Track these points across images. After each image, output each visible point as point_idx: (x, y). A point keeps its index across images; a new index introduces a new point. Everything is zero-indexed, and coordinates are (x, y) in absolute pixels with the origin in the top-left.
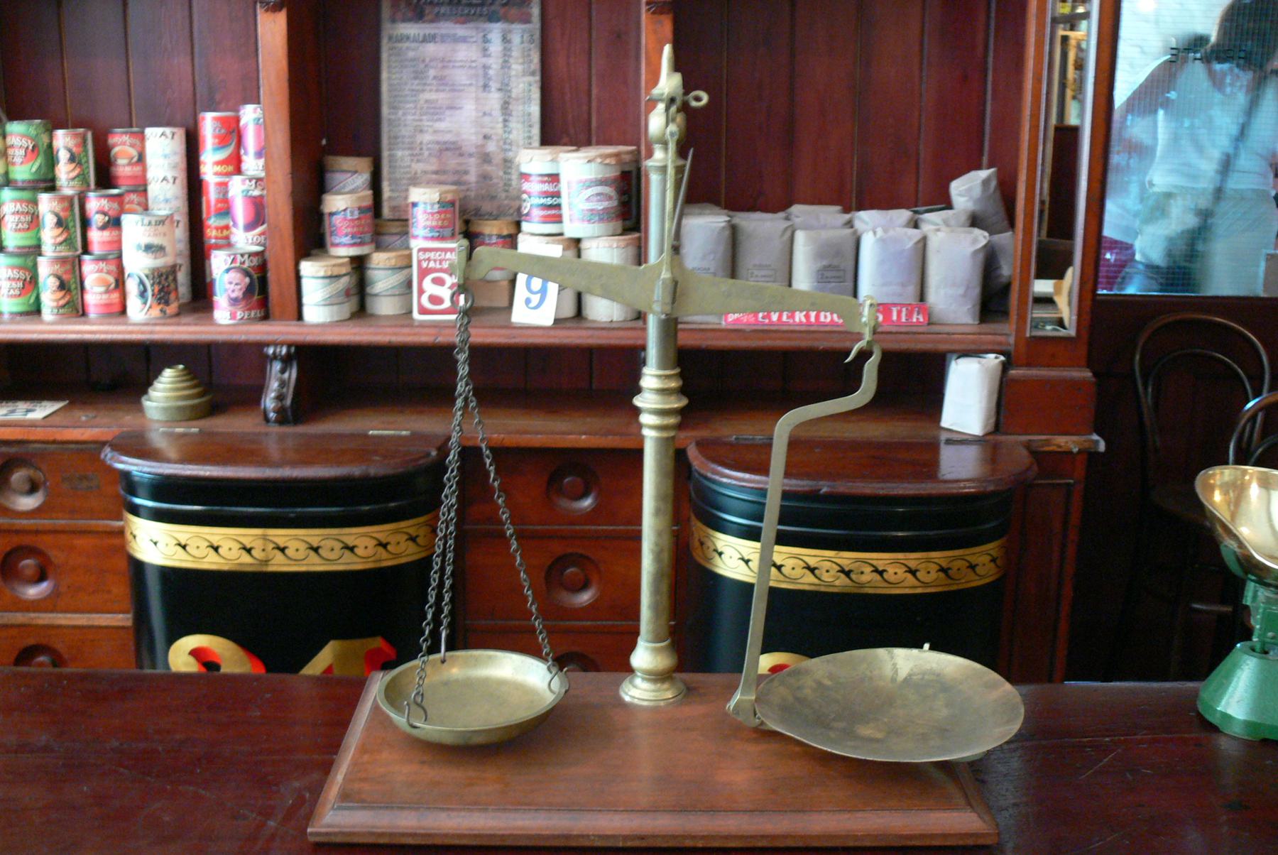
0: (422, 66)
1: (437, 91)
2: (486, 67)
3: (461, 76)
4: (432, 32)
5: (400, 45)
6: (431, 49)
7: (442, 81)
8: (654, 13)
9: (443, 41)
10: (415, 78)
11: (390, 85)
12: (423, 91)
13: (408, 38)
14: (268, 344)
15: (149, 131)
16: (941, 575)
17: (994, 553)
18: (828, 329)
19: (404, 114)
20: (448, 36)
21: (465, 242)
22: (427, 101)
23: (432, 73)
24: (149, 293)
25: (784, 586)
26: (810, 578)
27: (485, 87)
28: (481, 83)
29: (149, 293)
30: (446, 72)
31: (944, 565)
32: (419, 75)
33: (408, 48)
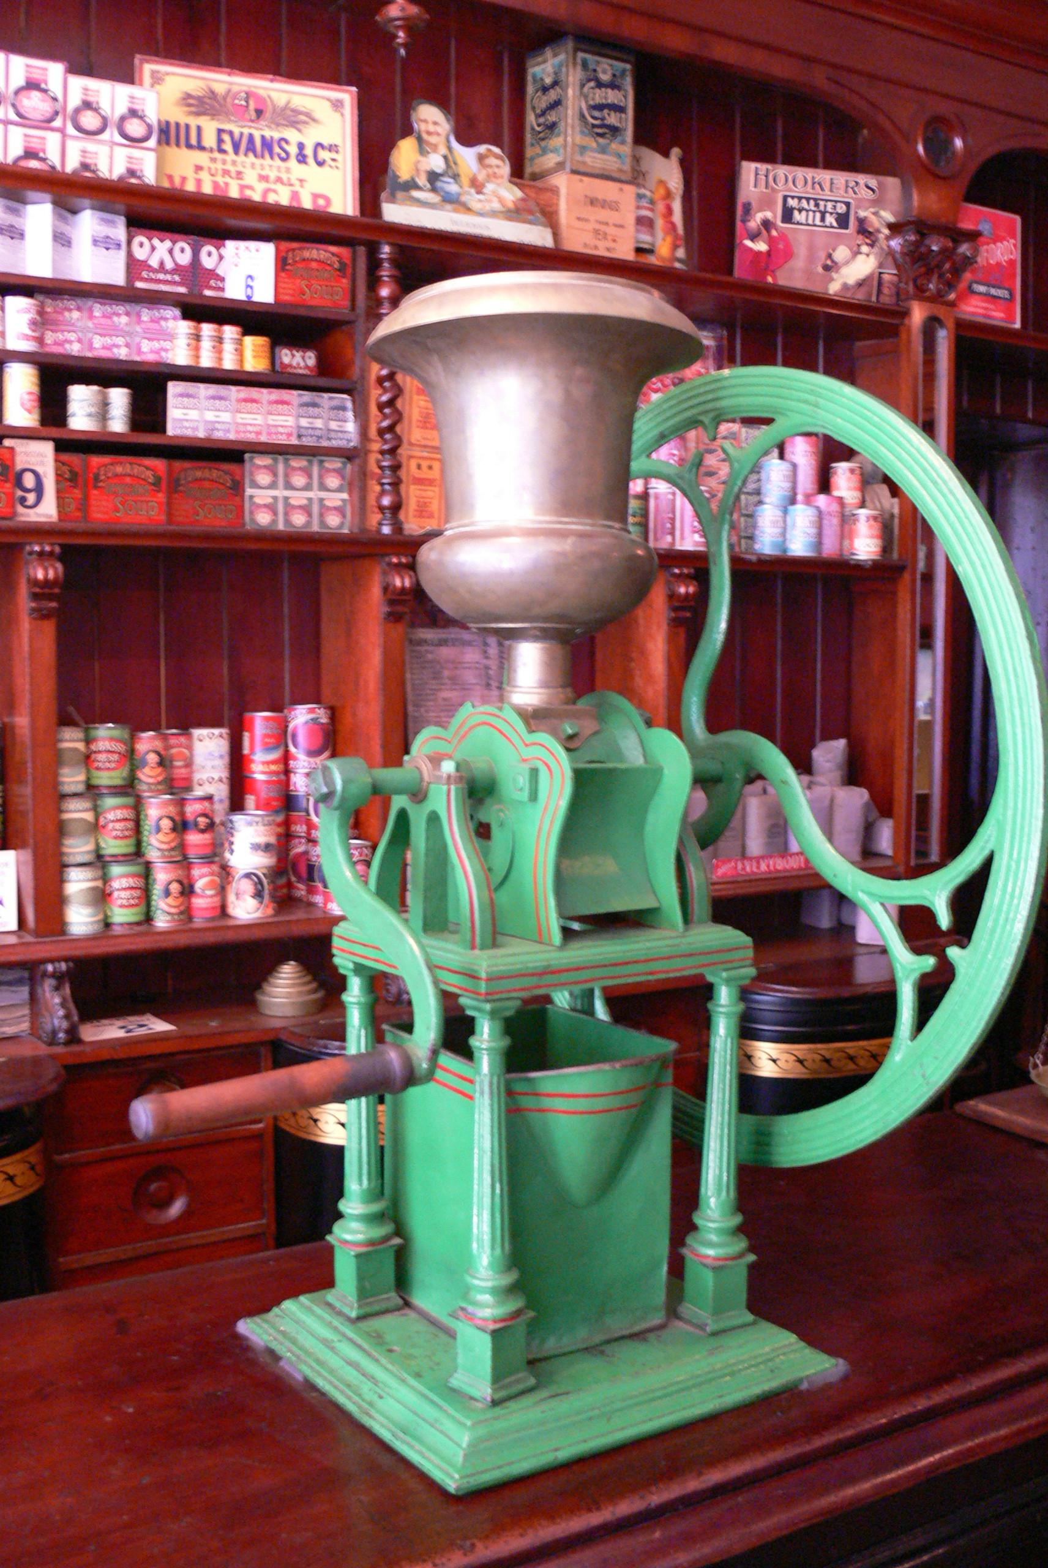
0: (438, 667)
1: (452, 690)
2: (487, 668)
3: (470, 677)
4: (444, 636)
5: (419, 648)
6: (445, 652)
7: (453, 679)
8: (35, 619)
9: (454, 645)
10: (434, 678)
11: (413, 684)
12: (440, 690)
13: (425, 641)
14: (44, 961)
15: (197, 732)
16: (825, 1065)
17: (33, 1159)
18: (781, 875)
19: (427, 711)
20: (457, 640)
21: (103, 852)
22: (445, 699)
23: (446, 673)
24: (266, 892)
25: (831, 1076)
26: (852, 1066)
27: (488, 685)
28: (484, 682)
29: (266, 892)
30: (458, 672)
31: (828, 1056)
32: (437, 676)
33: (427, 651)
